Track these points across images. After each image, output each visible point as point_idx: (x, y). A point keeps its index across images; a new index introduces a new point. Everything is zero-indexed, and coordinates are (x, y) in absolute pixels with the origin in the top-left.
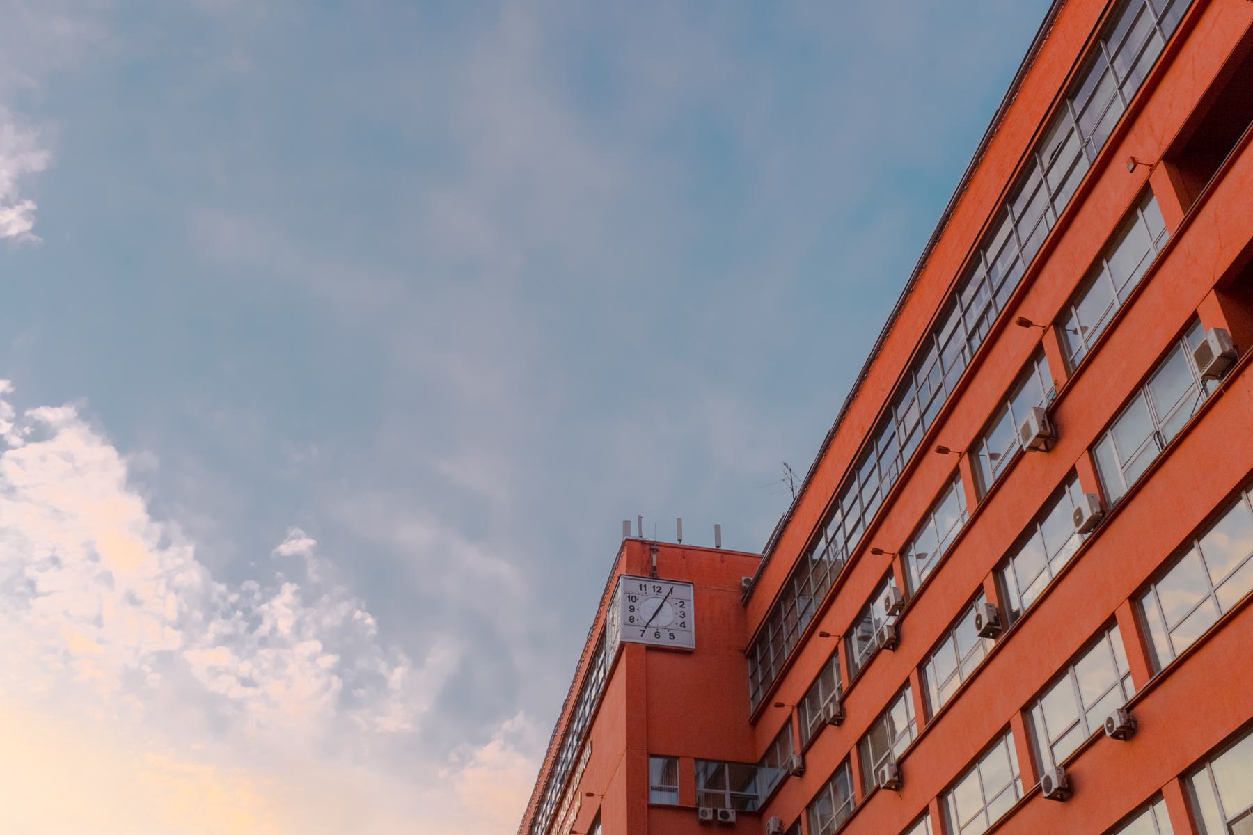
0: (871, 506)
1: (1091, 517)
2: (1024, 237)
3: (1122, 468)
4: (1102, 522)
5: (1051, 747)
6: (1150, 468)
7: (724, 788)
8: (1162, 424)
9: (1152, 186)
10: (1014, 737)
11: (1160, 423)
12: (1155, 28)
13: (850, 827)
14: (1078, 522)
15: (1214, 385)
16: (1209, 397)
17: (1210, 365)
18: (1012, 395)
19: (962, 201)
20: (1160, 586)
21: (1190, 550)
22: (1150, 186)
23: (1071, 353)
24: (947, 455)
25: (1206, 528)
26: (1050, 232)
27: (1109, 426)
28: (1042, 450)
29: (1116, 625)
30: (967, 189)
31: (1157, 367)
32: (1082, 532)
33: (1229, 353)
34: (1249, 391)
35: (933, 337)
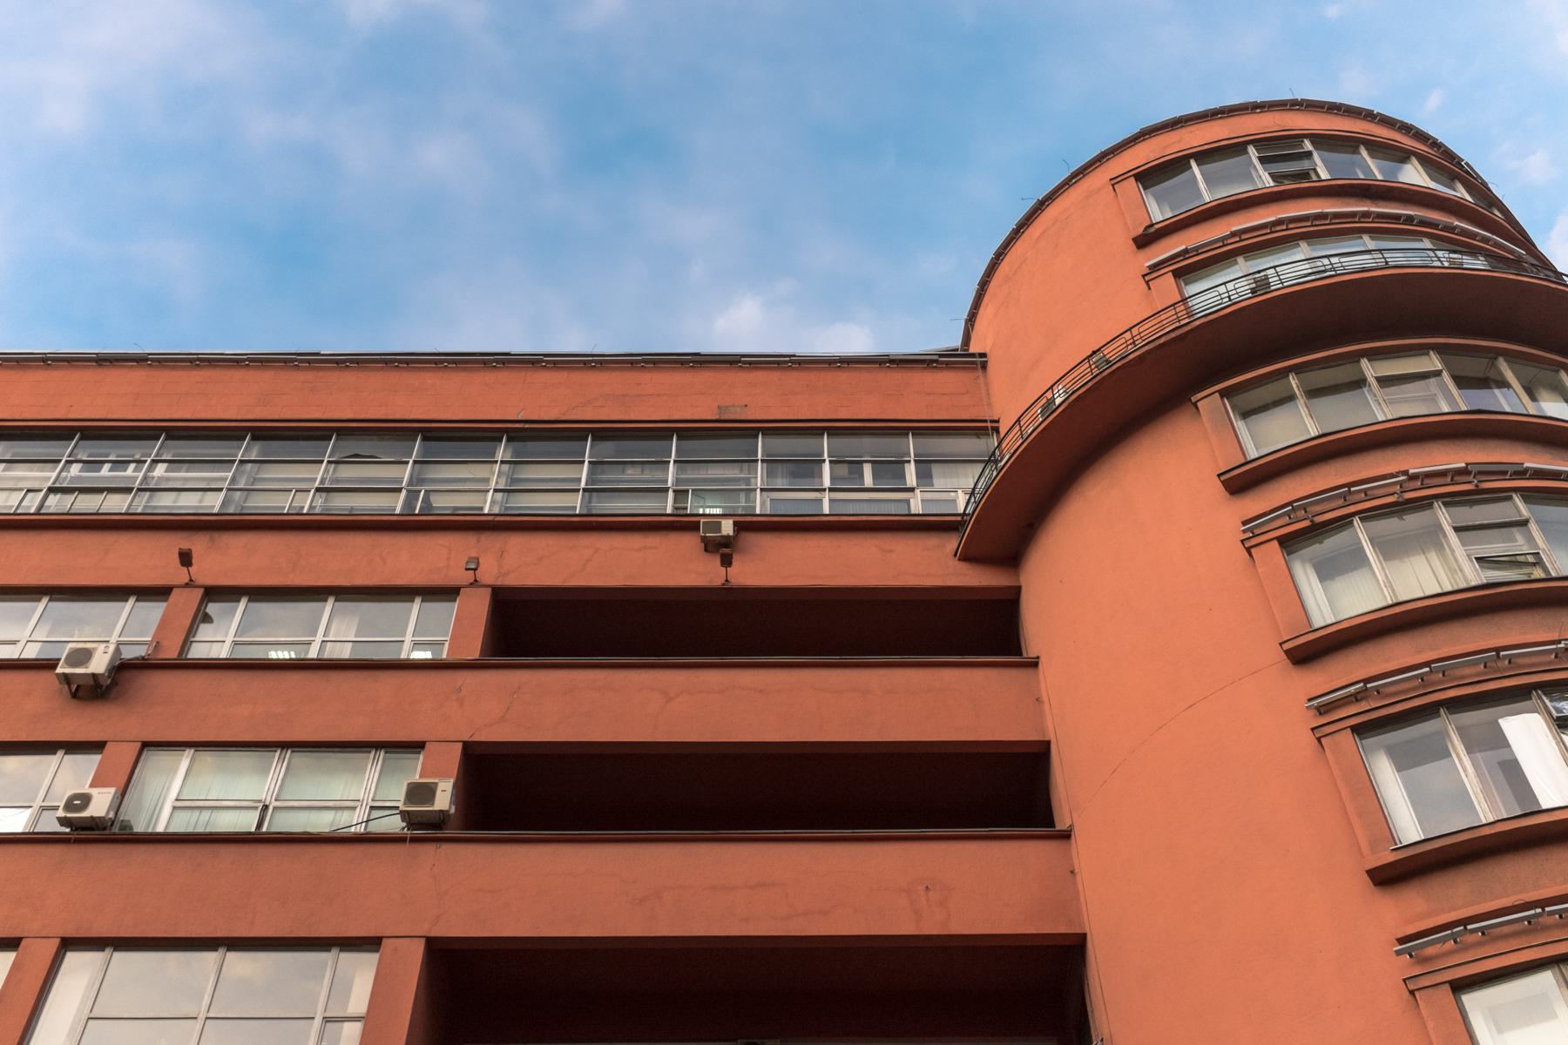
0: (1491, 409)
1: (99, 818)
2: (1022, 424)
3: (177, 800)
4: (97, 832)
5: (207, 1018)
6: (237, 834)
7: (700, 522)
8: (278, 804)
9: (172, 595)
10: (16, 958)
11: (276, 800)
12: (133, 488)
13: (1463, 966)
14: (69, 806)
15: (394, 824)
16: (123, 832)
18: (343, 596)
19: (85, 367)
20: (118, 956)
21: (98, 950)
22: (170, 594)
23: (194, 636)
24: (179, 565)
25: (246, 946)
26: (14, 514)
27: (198, 746)
28: (70, 690)
29: (16, 951)
30: (49, 364)
31: (321, 747)
32: (64, 822)
33: (449, 815)
34: (434, 865)
35: (75, 436)
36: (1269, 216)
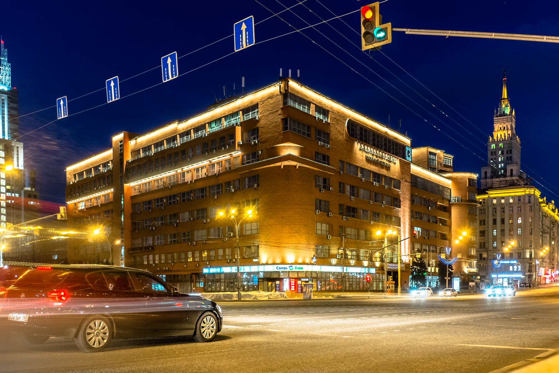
17: (308, 159)
36: (505, 368)
